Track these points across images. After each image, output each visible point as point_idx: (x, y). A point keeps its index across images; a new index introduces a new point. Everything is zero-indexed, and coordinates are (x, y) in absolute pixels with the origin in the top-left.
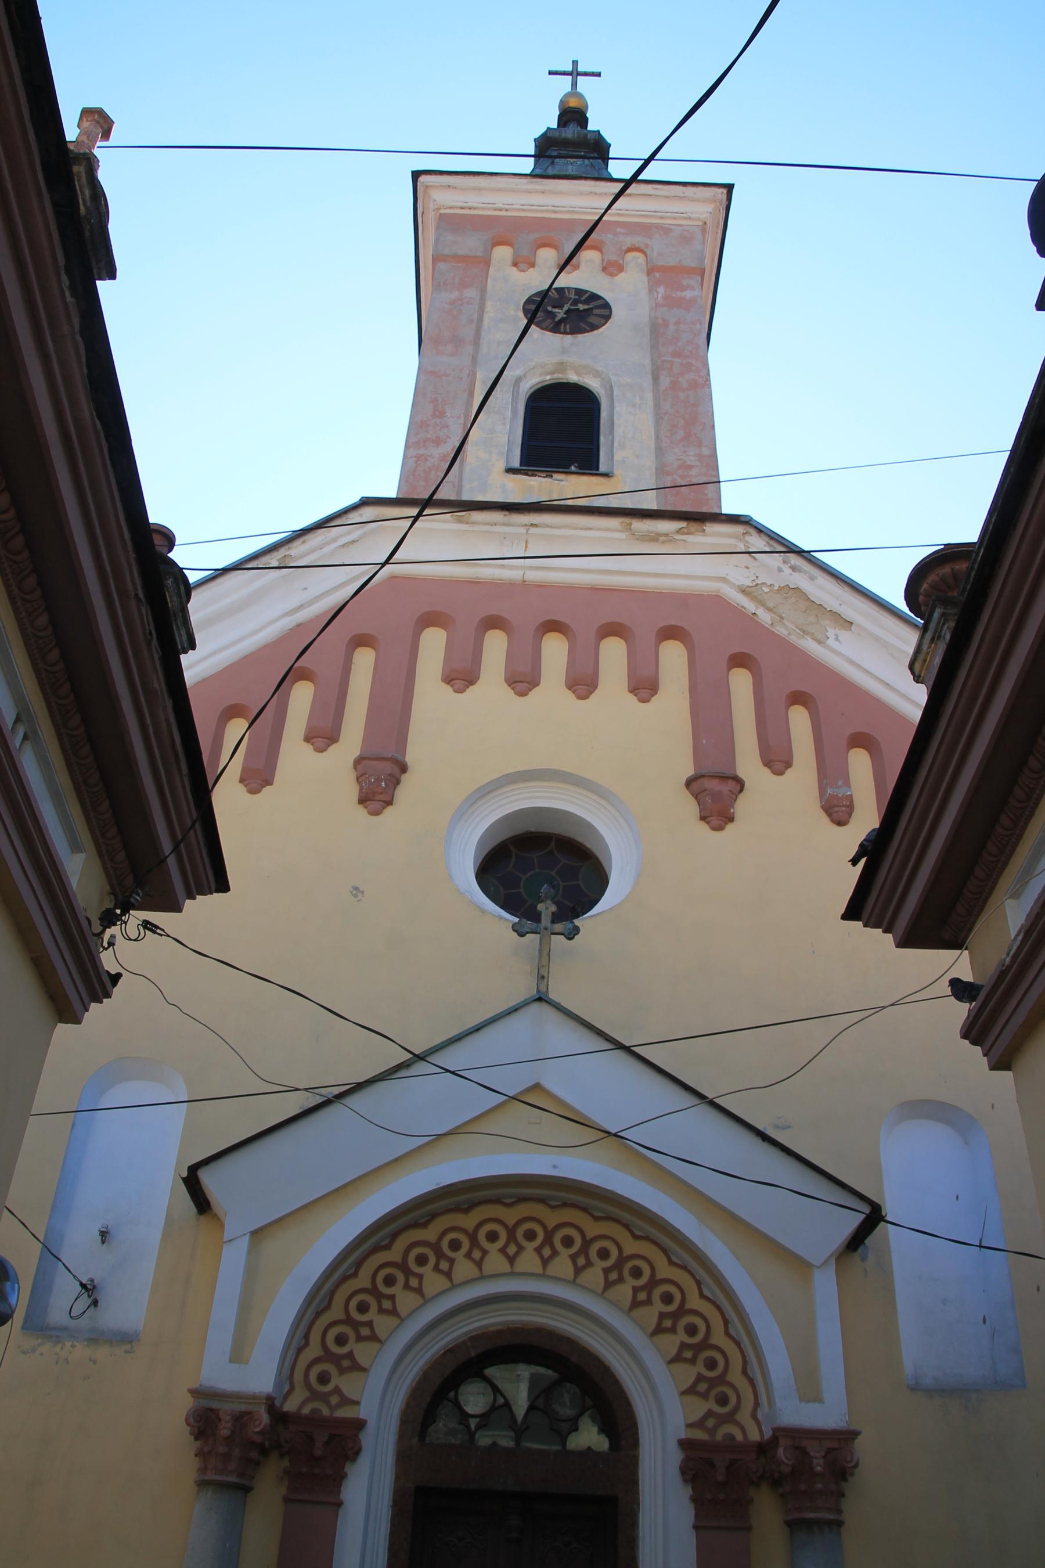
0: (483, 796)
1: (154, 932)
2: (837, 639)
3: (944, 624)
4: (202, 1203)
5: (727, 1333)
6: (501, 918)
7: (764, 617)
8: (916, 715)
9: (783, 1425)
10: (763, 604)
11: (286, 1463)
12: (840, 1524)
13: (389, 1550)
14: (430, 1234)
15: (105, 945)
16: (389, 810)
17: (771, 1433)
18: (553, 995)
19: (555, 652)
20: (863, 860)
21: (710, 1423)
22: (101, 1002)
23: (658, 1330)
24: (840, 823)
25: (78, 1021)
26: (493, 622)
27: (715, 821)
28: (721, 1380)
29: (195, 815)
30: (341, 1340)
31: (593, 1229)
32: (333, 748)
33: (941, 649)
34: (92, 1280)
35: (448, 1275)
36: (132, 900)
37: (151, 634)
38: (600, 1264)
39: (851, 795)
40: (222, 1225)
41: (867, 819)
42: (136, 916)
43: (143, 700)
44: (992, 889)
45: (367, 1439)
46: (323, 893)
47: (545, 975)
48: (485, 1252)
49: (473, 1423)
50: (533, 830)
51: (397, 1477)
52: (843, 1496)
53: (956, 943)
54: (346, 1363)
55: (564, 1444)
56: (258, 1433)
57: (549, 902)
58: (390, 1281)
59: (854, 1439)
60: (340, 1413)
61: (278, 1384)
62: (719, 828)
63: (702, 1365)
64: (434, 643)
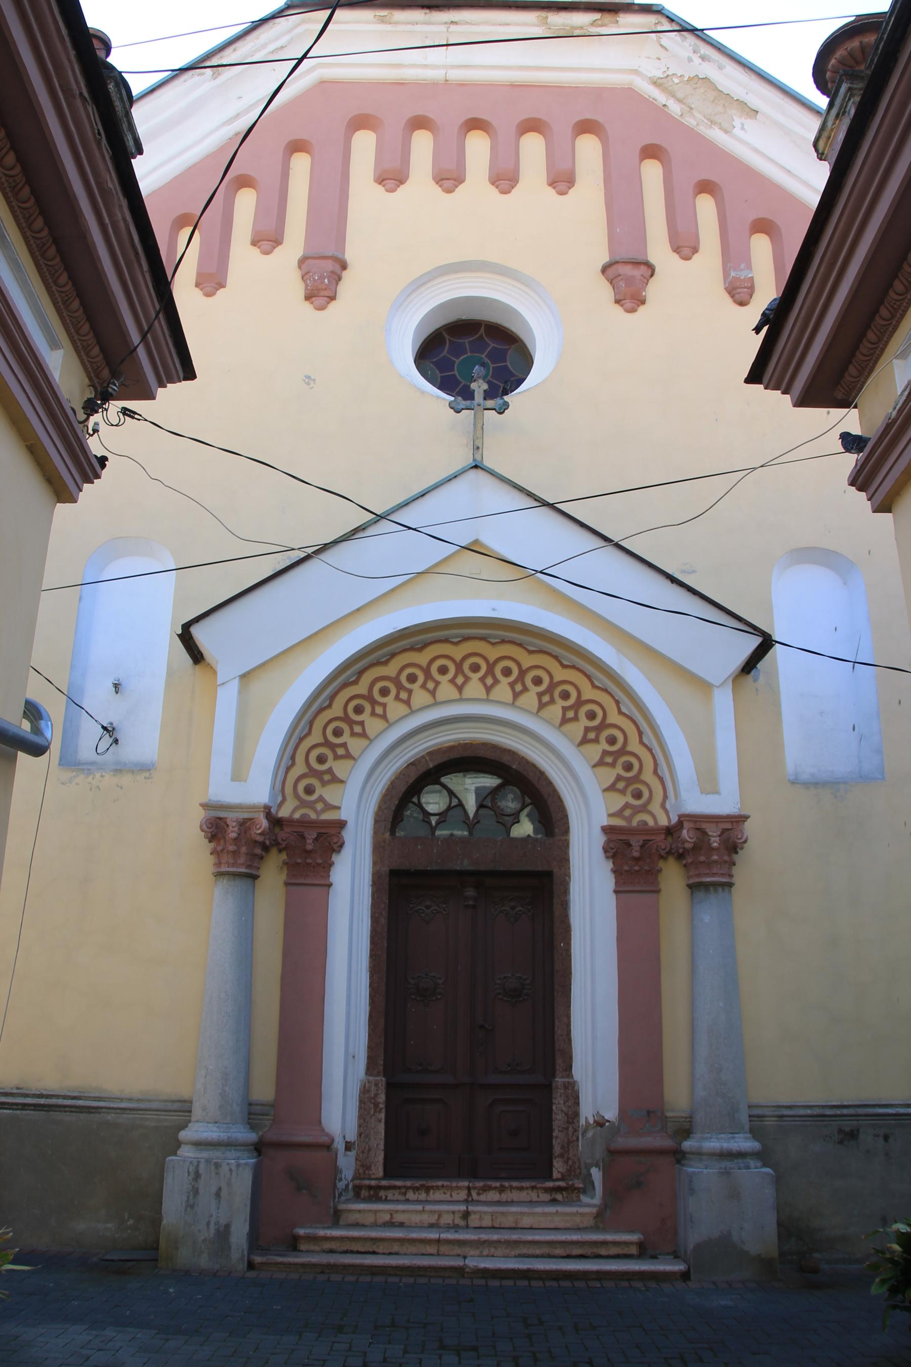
0: (419, 287)
1: (133, 418)
2: (742, 128)
3: (849, 99)
4: (196, 656)
5: (641, 742)
6: (438, 397)
7: (675, 108)
8: (814, 200)
9: (687, 812)
10: (672, 95)
11: (284, 856)
12: (730, 885)
13: (372, 917)
14: (391, 670)
15: (91, 432)
16: (333, 304)
17: (677, 818)
18: (487, 463)
19: (478, 148)
20: (766, 328)
21: (627, 813)
22: (93, 483)
23: (584, 741)
24: (742, 304)
25: (74, 500)
26: (419, 123)
27: (629, 304)
28: (637, 779)
29: (158, 307)
30: (321, 759)
31: (527, 661)
32: (278, 250)
33: (846, 122)
34: (111, 724)
35: (408, 702)
36: (110, 390)
37: (99, 134)
38: (534, 690)
39: (752, 278)
40: (215, 672)
41: (767, 292)
42: (114, 406)
43: (99, 200)
44: (883, 350)
45: (348, 835)
46: (278, 377)
47: (480, 446)
48: (437, 683)
49: (434, 820)
50: (464, 318)
51: (375, 863)
52: (734, 864)
53: (845, 403)
54: (327, 777)
55: (508, 832)
56: (260, 834)
57: (481, 381)
58: (359, 710)
59: (744, 821)
60: (326, 816)
61: (272, 795)
62: (632, 310)
63: (621, 767)
64: (364, 144)
